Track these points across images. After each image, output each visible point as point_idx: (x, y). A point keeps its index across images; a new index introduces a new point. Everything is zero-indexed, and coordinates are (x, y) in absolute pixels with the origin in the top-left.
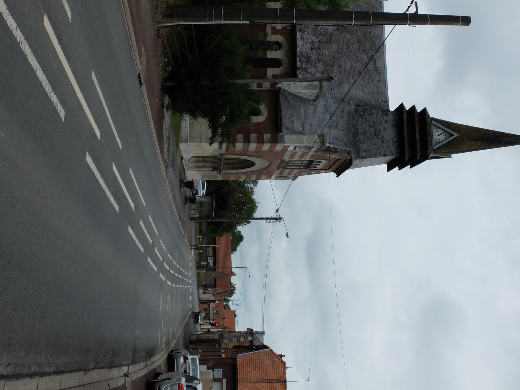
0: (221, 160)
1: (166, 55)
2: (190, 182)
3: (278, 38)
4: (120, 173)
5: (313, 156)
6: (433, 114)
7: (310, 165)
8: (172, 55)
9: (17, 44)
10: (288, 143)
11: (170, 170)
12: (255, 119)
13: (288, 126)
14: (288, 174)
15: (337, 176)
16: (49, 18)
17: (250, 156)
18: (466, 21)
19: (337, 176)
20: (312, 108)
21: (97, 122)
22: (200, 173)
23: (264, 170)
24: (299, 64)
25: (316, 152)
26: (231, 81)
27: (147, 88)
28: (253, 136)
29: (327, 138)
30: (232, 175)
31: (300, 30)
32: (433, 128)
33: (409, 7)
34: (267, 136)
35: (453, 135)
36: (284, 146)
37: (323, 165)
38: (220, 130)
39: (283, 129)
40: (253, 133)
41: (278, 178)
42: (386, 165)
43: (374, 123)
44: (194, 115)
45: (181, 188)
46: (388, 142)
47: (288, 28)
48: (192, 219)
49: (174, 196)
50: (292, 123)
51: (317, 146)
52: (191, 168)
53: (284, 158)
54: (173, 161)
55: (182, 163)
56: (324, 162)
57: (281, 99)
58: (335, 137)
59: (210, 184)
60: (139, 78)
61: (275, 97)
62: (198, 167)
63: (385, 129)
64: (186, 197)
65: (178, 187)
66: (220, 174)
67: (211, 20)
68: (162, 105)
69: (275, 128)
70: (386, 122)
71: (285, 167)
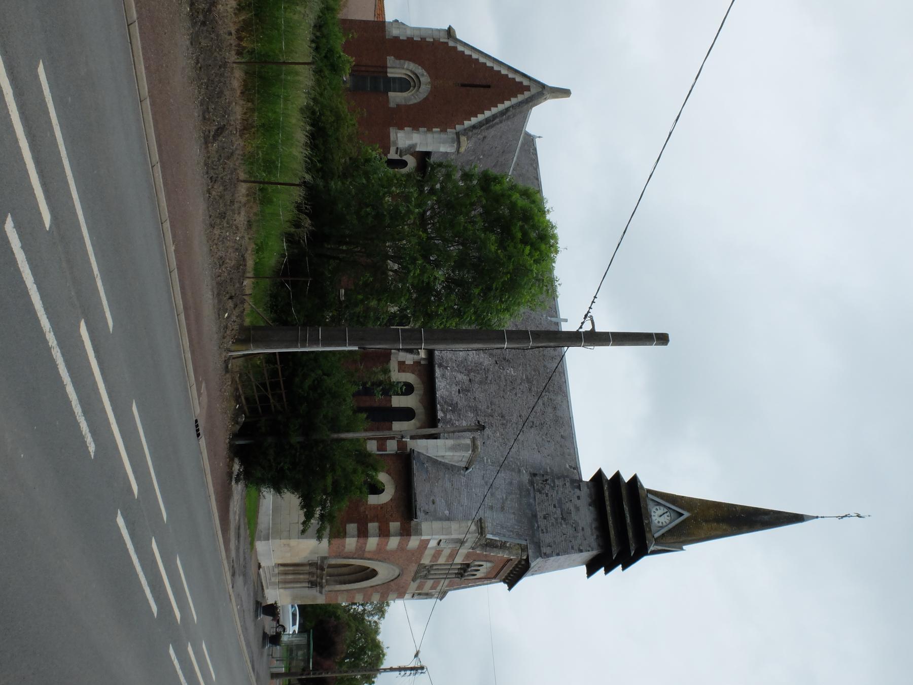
0: (322, 569)
1: (237, 399)
2: (272, 605)
3: (410, 378)
4: (162, 557)
5: (468, 556)
6: (647, 483)
7: (465, 571)
8: (247, 399)
9: (49, 349)
10: (428, 535)
11: (240, 580)
12: (373, 500)
13: (426, 507)
14: (432, 588)
15: (510, 589)
16: (86, 323)
17: (369, 559)
18: (663, 339)
19: (510, 589)
20: (463, 480)
21: (134, 472)
22: (288, 592)
23: (392, 583)
24: (440, 415)
25: (473, 548)
26: (335, 436)
27: (208, 444)
28: (373, 526)
29: (489, 525)
30: (342, 596)
31: (440, 365)
32: (651, 505)
33: (583, 323)
34: (394, 526)
35: (681, 515)
36: (422, 541)
37: (485, 571)
38: (318, 512)
39: (418, 513)
40: (372, 521)
41: (416, 597)
42: (584, 567)
43: (560, 501)
44: (278, 490)
45: (256, 616)
46: (583, 529)
47: (422, 362)
48: (274, 676)
49: (245, 629)
50: (434, 503)
51: (472, 538)
52: (274, 584)
53: (422, 562)
54: (245, 567)
55: (259, 575)
56: (486, 567)
57: (415, 467)
58: (501, 525)
59: (309, 614)
60: (197, 426)
61: (405, 465)
62: (285, 582)
63: (577, 509)
64: (265, 635)
65: (252, 614)
66: (321, 592)
67: (304, 346)
68: (230, 474)
69: (407, 510)
70: (579, 498)
71: (425, 577)
